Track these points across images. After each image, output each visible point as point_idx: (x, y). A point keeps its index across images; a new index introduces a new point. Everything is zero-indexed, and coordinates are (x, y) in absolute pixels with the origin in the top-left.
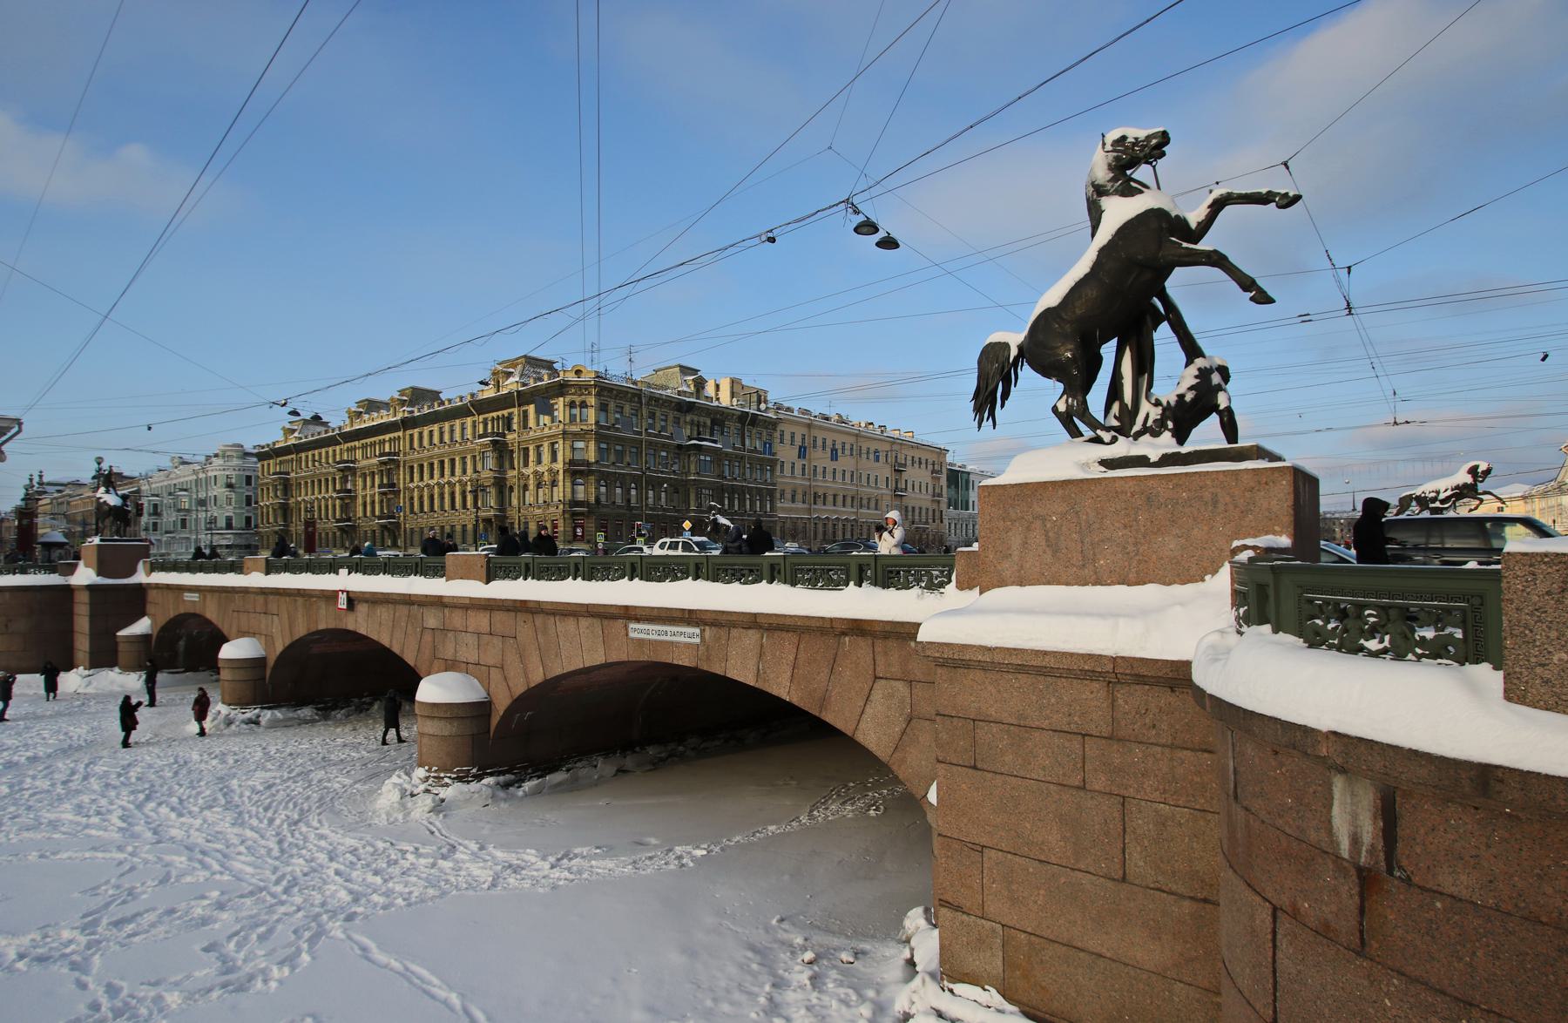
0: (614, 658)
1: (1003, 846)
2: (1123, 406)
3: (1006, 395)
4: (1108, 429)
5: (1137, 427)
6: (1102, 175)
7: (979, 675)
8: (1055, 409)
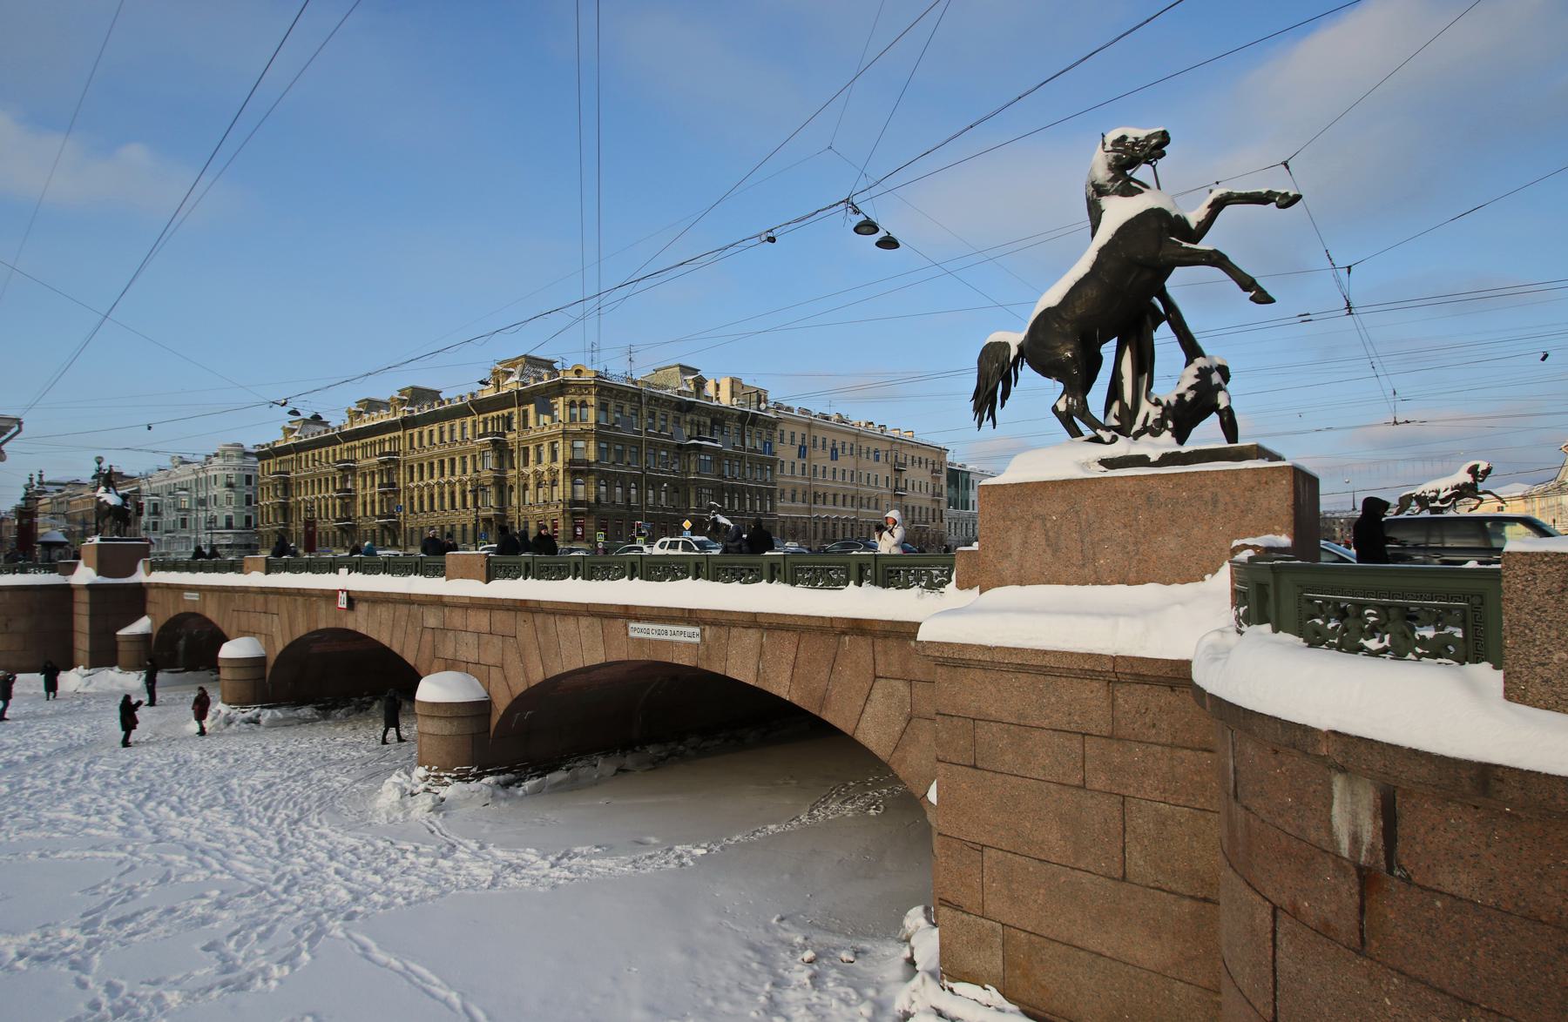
0: (614, 657)
1: (1003, 845)
2: (1123, 405)
3: (1006, 395)
4: (1108, 429)
5: (1137, 427)
6: (1102, 174)
7: (979, 674)
8: (1055, 409)
